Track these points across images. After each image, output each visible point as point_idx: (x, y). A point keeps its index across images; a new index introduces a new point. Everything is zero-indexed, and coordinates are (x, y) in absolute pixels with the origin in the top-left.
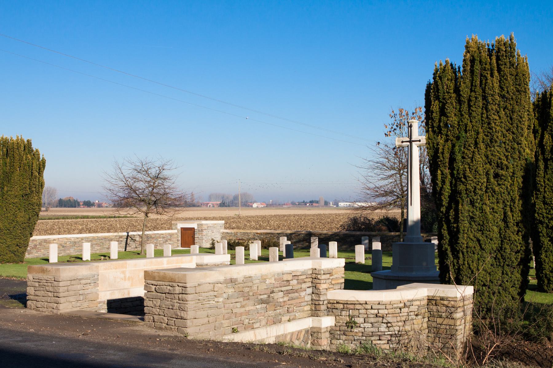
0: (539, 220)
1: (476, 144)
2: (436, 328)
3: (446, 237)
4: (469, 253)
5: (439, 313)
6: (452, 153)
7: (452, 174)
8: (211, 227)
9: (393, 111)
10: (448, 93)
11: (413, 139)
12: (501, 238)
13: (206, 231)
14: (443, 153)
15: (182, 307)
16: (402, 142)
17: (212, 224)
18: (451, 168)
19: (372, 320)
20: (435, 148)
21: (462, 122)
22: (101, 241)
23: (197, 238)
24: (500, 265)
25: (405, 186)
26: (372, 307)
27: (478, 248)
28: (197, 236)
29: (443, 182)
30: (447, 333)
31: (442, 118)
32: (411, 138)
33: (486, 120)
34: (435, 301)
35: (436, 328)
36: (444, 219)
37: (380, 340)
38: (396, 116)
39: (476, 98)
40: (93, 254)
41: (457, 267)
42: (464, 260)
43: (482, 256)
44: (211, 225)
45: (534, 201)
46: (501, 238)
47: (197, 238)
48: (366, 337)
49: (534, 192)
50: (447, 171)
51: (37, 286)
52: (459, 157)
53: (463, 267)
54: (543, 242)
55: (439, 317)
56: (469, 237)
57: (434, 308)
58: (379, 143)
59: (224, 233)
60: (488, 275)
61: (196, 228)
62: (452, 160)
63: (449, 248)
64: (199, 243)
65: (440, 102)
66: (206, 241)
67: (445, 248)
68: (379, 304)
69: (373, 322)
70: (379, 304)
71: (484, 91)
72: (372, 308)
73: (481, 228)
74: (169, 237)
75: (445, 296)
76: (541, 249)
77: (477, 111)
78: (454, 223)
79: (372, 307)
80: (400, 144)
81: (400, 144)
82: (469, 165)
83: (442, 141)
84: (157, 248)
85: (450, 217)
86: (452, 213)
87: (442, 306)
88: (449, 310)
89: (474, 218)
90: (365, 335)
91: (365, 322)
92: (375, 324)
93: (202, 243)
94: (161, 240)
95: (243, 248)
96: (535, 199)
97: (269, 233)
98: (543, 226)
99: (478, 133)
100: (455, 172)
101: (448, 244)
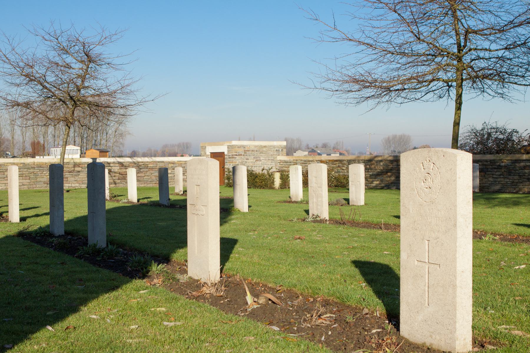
8: (253, 151)
22: (32, 170)
25: (76, 136)
40: (182, 247)
59: (281, 161)
61: (226, 153)
95: (17, 167)
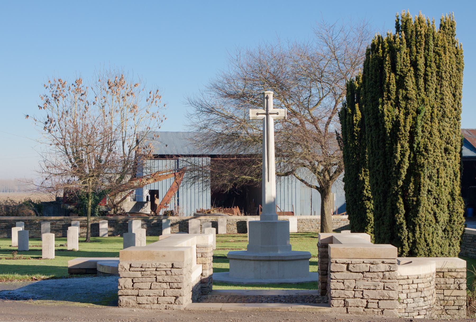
0: (368, 196)
1: (432, 118)
2: (444, 300)
3: (402, 210)
4: (426, 226)
5: (447, 285)
6: (414, 127)
7: (411, 147)
9: (49, 81)
10: (406, 66)
11: (270, 112)
12: (450, 210)
14: (405, 126)
15: (389, 287)
16: (257, 114)
18: (411, 141)
19: (414, 295)
20: (394, 121)
21: (420, 96)
24: (448, 237)
26: (413, 282)
27: (434, 221)
29: (403, 155)
30: (455, 304)
31: (400, 90)
32: (267, 111)
33: (440, 96)
34: (442, 273)
35: (444, 300)
36: (400, 193)
37: (419, 315)
38: (52, 87)
39: (432, 73)
41: (411, 241)
42: (421, 233)
43: (436, 229)
45: (363, 178)
46: (450, 210)
48: (408, 313)
49: (363, 169)
50: (407, 145)
51: (140, 276)
52: (419, 130)
53: (419, 240)
54: (370, 218)
55: (446, 288)
56: (427, 210)
57: (442, 280)
58: (28, 116)
60: (440, 248)
62: (413, 134)
63: (404, 222)
65: (396, 74)
67: (400, 221)
68: (418, 278)
69: (414, 297)
70: (418, 278)
71: (438, 67)
72: (413, 283)
73: (436, 201)
75: (453, 267)
76: (367, 226)
77: (433, 85)
78: (414, 196)
79: (413, 282)
80: (255, 116)
81: (255, 116)
82: (428, 139)
83: (402, 116)
85: (410, 190)
86: (412, 186)
87: (450, 277)
88: (457, 281)
89: (432, 191)
90: (408, 311)
91: (407, 298)
92: (416, 299)
96: (363, 176)
98: (371, 203)
99: (433, 108)
100: (415, 146)
101: (403, 218)
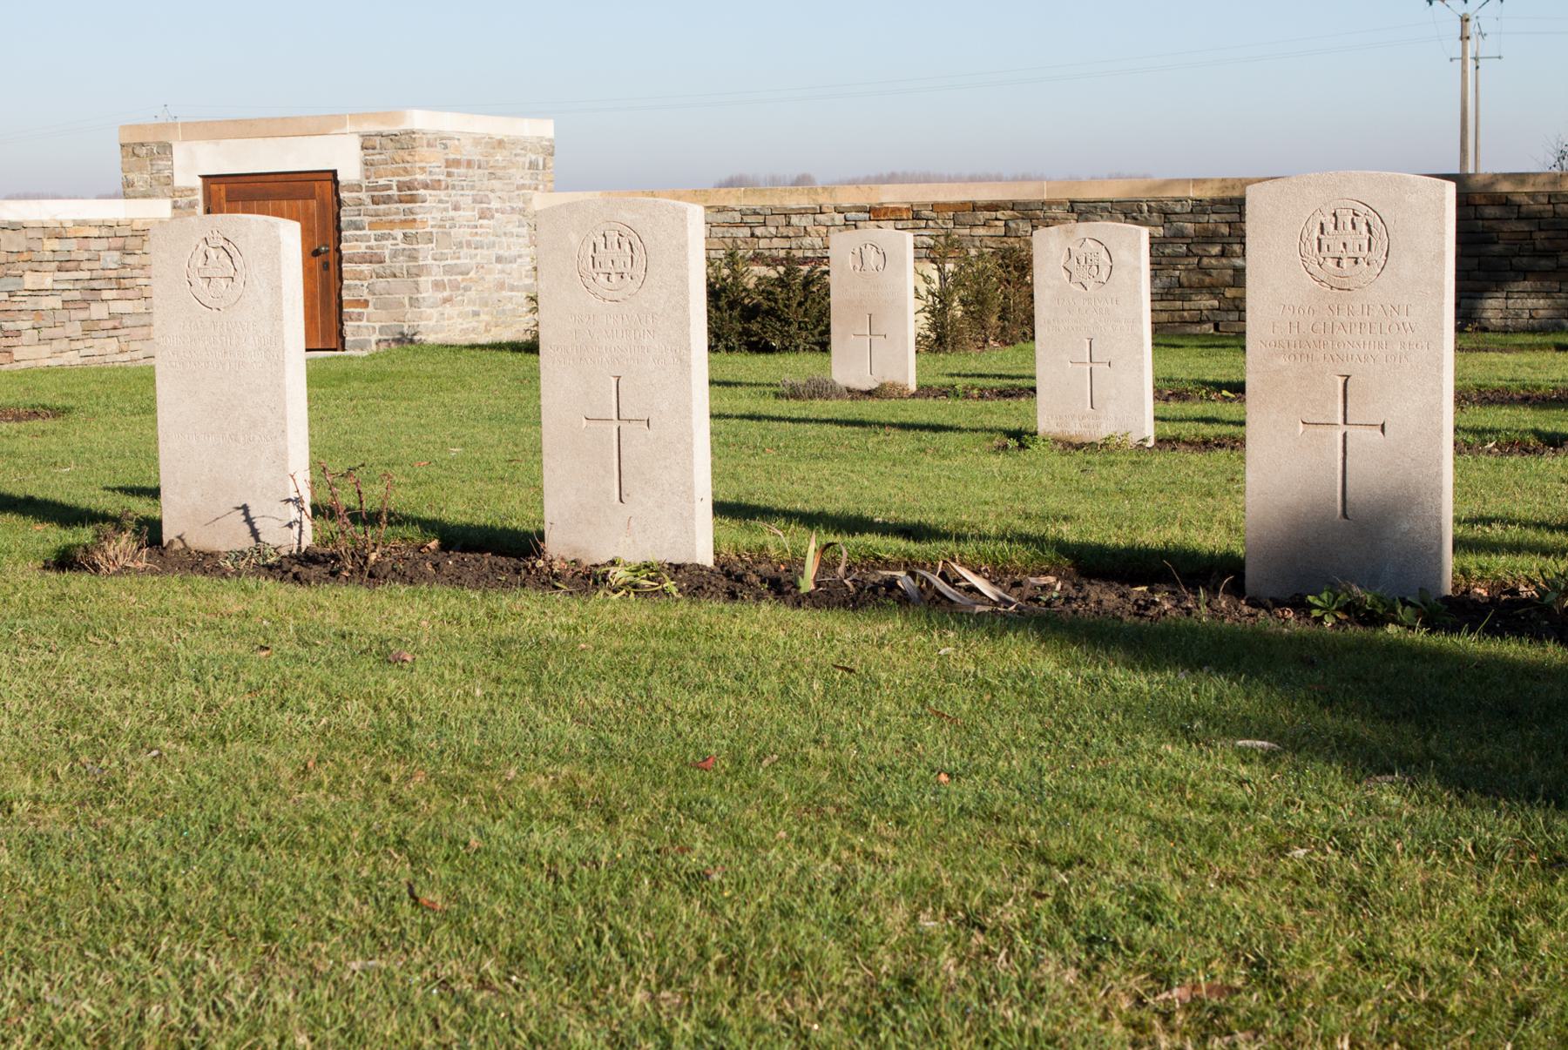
8: (469, 164)
13: (442, 194)
17: (477, 141)
23: (364, 259)
28: (361, 248)
44: (469, 152)
47: (364, 259)
61: (350, 173)
64: (384, 306)
66: (438, 285)
74: (111, 260)
84: (18, 354)
93: (414, 302)
94: (47, 281)
97: (993, 207)
